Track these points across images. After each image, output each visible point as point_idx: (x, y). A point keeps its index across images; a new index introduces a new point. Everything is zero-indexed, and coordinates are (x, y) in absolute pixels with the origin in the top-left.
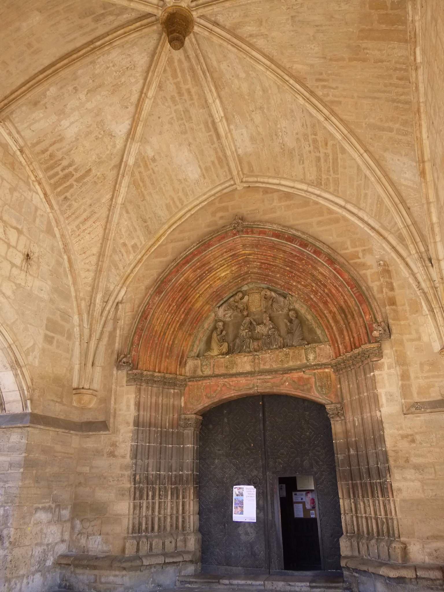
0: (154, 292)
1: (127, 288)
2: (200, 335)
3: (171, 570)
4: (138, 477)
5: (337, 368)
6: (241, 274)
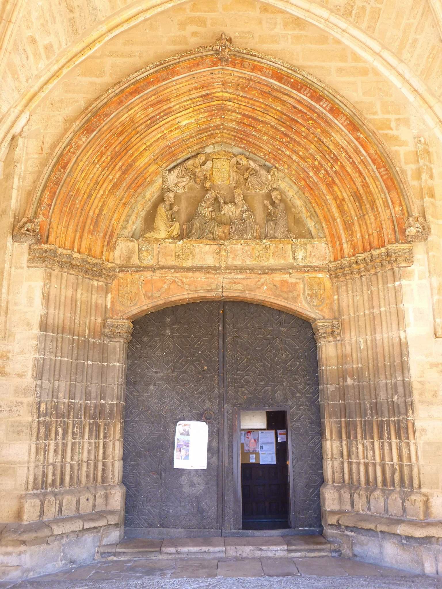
0: (80, 128)
1: (30, 115)
2: (139, 207)
3: (89, 538)
4: (43, 407)
5: (337, 273)
6: (211, 127)
